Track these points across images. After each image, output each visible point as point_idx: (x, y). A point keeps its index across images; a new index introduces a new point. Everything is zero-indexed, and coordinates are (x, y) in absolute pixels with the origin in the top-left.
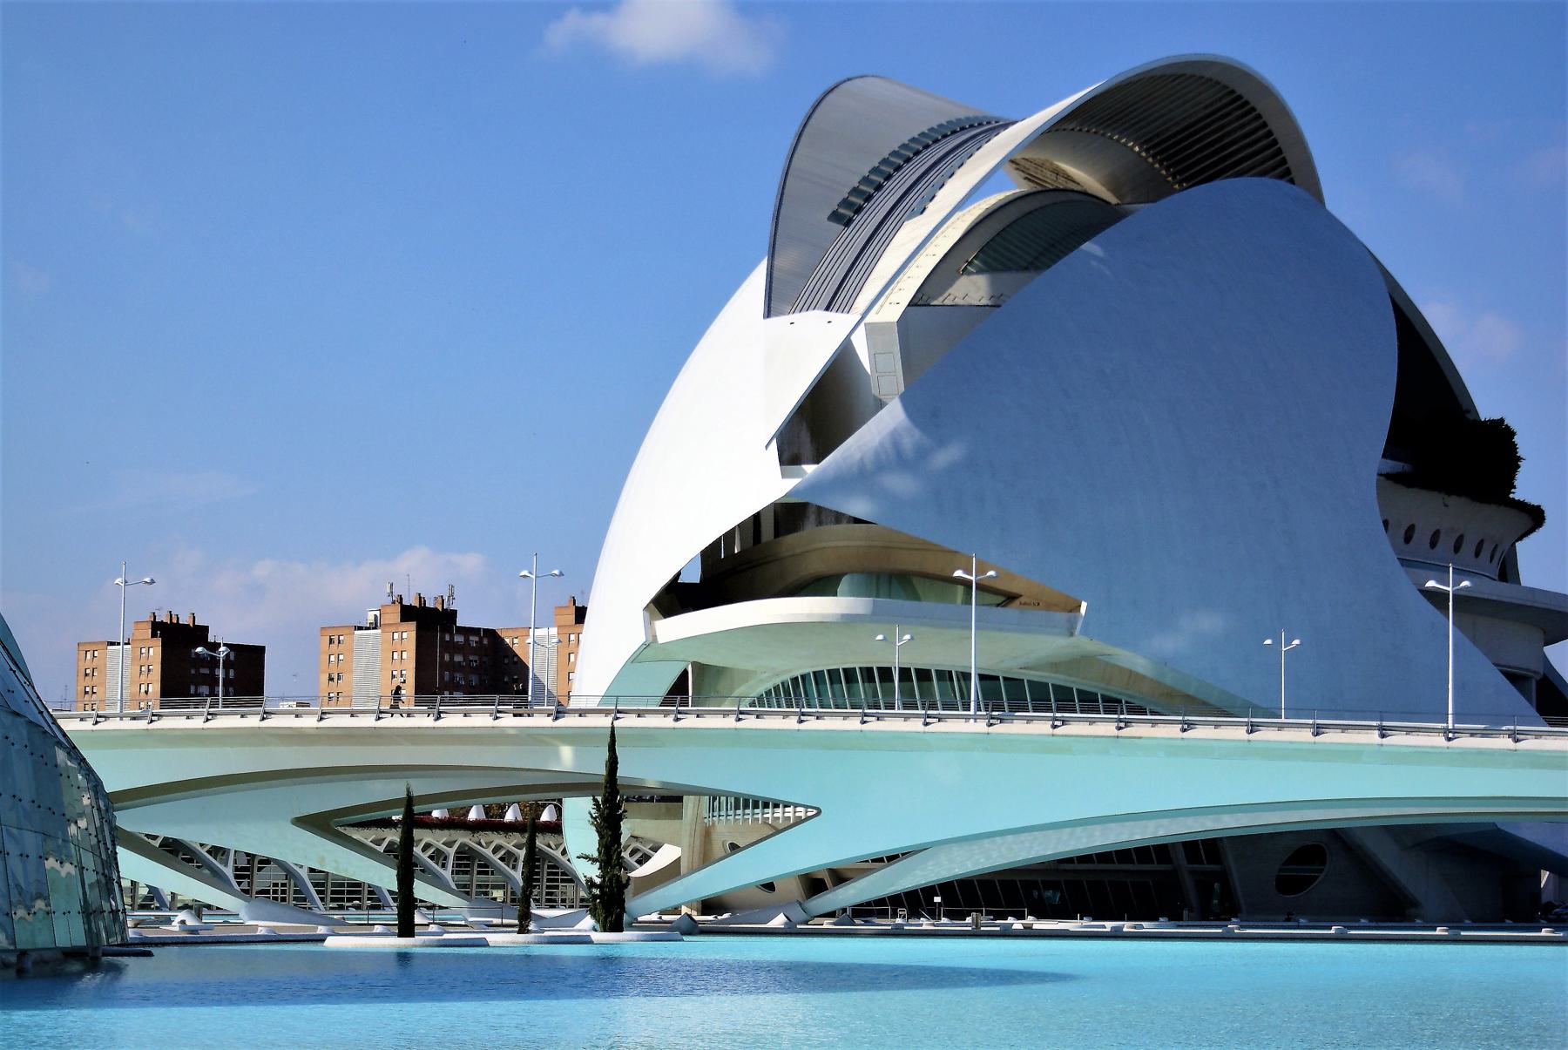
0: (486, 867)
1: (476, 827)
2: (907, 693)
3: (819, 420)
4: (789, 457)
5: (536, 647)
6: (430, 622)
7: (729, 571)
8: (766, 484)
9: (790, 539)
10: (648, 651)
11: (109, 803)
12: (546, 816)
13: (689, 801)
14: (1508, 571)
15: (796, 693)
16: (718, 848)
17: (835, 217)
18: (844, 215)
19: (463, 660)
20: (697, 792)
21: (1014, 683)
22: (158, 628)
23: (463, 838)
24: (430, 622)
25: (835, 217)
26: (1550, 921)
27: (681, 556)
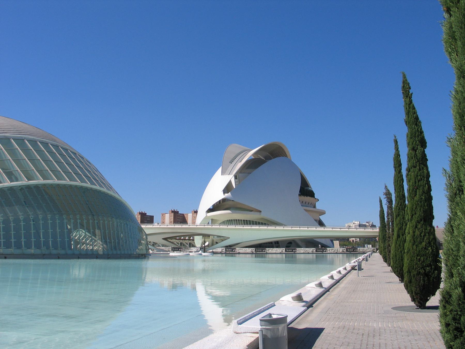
0: (184, 245)
1: (182, 239)
2: (237, 223)
3: (228, 189)
4: (224, 193)
5: (189, 217)
6: (175, 213)
7: (215, 208)
8: (221, 196)
9: (225, 203)
10: (206, 218)
11: (147, 235)
12: (191, 238)
13: (211, 236)
14: (315, 207)
15: (224, 223)
16: (214, 243)
17: (230, 162)
18: (231, 162)
19: (179, 218)
20: (212, 235)
21: (253, 221)
22: (140, 213)
23: (181, 241)
24: (175, 213)
25: (230, 162)
26: (419, 302)
27: (210, 206)
